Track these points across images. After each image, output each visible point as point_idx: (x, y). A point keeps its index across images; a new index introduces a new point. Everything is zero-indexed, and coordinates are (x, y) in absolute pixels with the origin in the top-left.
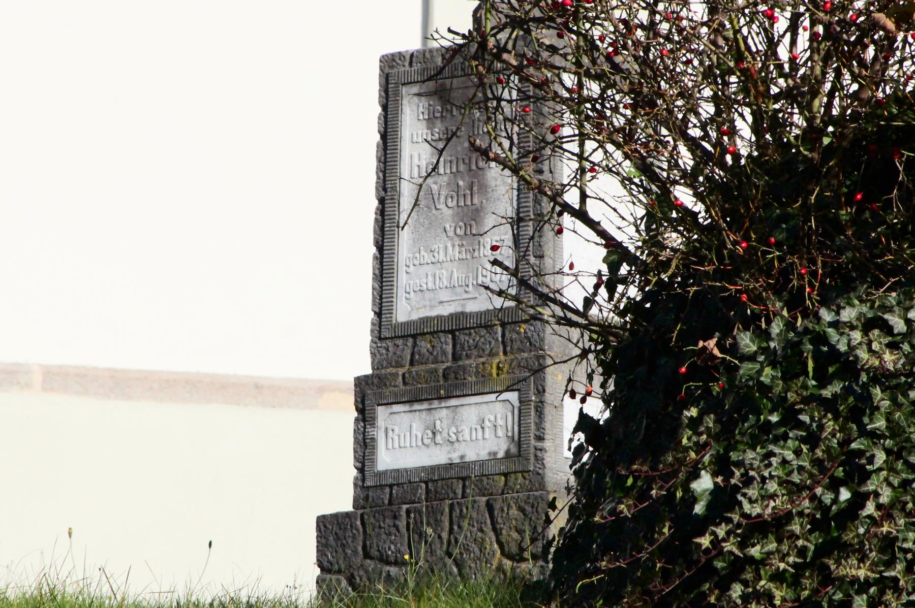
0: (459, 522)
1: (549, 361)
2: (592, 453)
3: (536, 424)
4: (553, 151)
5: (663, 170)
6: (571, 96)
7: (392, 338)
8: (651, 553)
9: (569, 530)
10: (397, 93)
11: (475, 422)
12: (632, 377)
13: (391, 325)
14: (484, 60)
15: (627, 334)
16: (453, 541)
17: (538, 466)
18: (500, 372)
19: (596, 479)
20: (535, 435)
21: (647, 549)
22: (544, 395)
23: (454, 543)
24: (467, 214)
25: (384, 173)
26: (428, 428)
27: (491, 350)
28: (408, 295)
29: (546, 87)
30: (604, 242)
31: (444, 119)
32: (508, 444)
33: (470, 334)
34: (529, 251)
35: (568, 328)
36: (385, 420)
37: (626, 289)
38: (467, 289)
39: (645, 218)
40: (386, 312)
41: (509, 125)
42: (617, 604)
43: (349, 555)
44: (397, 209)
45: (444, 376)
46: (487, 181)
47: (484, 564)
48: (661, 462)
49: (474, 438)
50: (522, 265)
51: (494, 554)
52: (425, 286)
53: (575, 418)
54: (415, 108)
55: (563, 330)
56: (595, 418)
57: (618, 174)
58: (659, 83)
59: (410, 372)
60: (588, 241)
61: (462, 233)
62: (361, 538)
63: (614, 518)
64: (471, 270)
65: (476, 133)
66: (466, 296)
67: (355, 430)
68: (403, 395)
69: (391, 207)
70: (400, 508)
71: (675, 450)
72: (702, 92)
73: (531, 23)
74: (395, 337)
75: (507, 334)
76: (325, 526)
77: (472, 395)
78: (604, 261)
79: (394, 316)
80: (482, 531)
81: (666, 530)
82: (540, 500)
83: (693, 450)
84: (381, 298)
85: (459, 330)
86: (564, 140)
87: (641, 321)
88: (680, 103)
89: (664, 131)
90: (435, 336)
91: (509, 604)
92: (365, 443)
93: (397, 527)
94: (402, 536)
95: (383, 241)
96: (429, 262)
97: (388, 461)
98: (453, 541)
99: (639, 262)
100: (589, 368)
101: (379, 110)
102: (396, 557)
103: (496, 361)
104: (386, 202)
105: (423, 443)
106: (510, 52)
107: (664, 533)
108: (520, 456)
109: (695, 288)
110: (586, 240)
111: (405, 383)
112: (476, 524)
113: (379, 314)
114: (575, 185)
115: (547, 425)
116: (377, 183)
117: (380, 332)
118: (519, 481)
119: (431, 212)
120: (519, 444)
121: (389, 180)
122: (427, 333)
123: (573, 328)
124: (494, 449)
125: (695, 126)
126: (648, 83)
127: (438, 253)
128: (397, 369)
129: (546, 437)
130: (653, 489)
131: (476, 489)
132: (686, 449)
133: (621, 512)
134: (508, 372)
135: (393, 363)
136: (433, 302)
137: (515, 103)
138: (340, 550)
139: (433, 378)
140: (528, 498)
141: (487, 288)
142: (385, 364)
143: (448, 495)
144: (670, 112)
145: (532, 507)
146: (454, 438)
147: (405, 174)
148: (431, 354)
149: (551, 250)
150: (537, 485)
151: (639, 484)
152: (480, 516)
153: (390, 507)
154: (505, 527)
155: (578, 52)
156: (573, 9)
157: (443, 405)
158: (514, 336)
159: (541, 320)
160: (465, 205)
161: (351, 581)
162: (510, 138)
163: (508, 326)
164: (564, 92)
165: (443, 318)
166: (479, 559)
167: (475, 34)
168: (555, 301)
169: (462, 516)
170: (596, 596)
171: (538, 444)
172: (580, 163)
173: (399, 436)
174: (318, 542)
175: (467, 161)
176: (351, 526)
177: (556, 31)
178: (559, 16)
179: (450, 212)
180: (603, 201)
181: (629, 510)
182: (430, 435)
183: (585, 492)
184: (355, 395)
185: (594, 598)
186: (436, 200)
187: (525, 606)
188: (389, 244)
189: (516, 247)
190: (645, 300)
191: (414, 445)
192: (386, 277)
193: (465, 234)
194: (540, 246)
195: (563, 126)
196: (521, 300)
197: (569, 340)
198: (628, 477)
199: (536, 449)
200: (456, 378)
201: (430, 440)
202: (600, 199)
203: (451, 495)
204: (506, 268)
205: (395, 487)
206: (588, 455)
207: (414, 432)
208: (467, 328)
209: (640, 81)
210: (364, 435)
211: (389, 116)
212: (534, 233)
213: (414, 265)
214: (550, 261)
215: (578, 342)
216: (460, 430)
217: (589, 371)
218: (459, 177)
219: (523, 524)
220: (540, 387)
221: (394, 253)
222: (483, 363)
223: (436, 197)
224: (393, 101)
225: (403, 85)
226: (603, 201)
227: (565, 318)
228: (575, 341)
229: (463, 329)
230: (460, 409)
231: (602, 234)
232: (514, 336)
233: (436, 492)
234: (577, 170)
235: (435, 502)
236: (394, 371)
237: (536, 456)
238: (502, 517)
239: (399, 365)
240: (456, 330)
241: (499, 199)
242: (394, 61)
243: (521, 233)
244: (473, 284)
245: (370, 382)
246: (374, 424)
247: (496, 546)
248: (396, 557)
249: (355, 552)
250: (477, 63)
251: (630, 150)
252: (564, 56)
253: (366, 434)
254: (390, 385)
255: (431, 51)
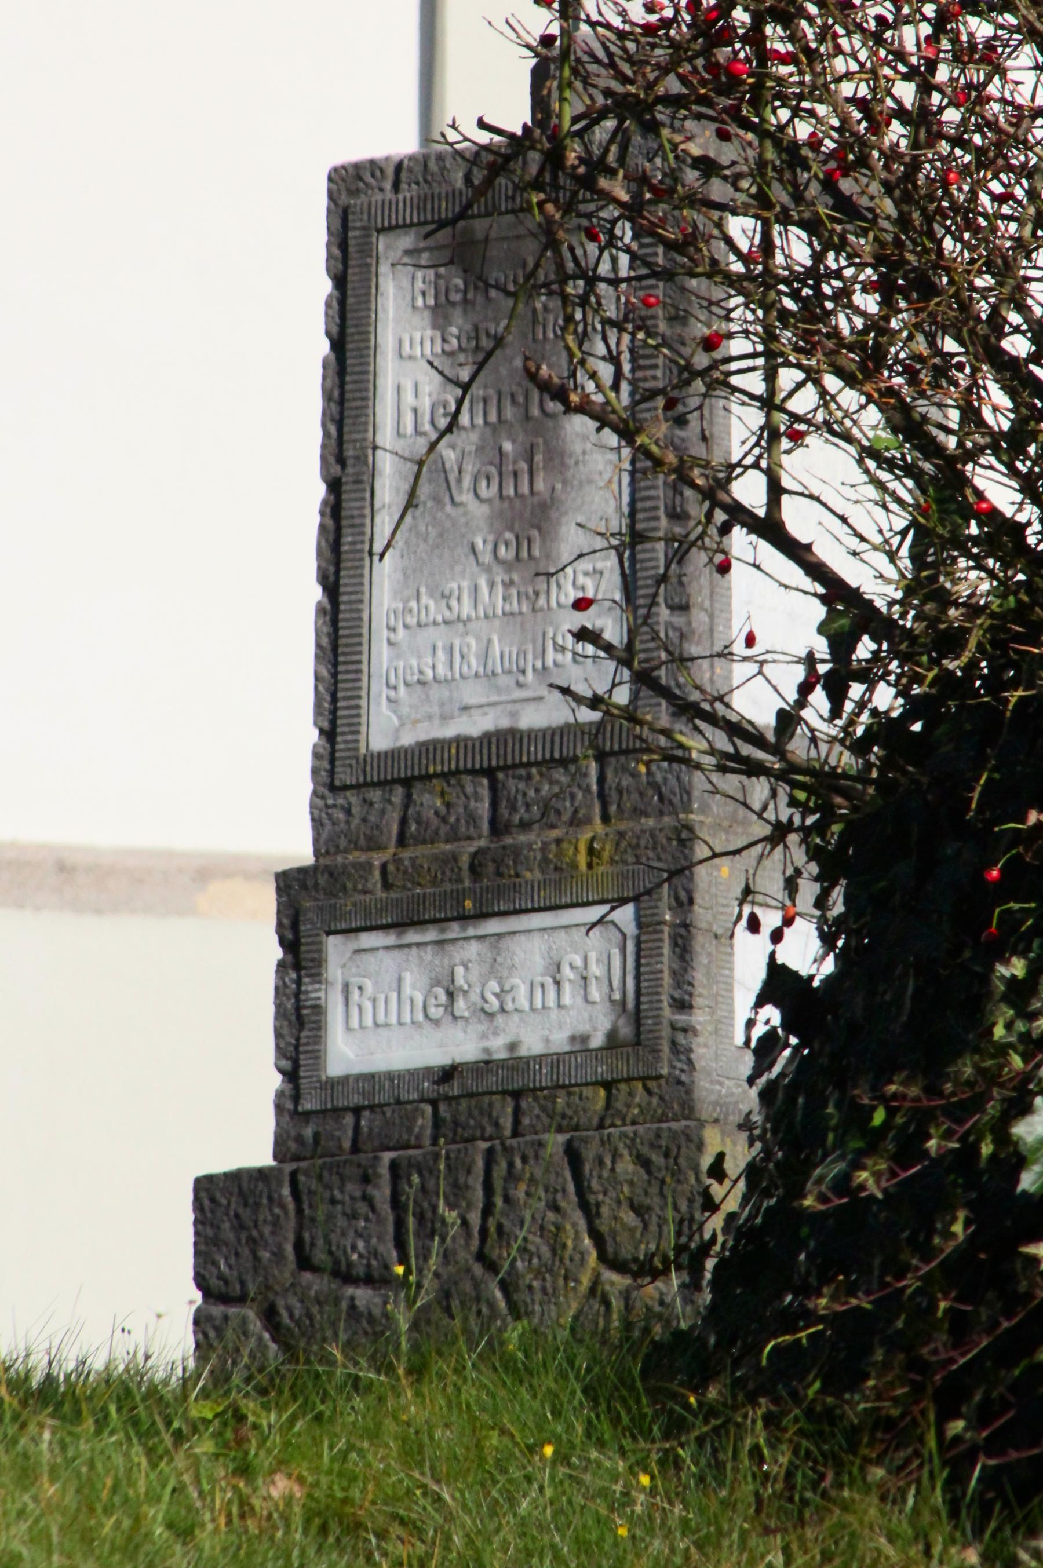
0: (505, 1189)
1: (701, 851)
2: (797, 1049)
3: (674, 973)
5: (949, 431)
7: (357, 787)
8: (927, 1279)
10: (367, 250)
12: (882, 884)
13: (357, 758)
15: (871, 790)
16: (492, 1229)
17: (679, 1065)
18: (595, 860)
20: (672, 997)
21: (917, 1269)
22: (690, 911)
23: (495, 1236)
26: (437, 983)
27: (576, 812)
28: (392, 693)
30: (821, 590)
31: (469, 307)
32: (613, 1017)
33: (529, 777)
35: (744, 778)
37: (871, 689)
39: (911, 533)
40: (346, 729)
41: (612, 335)
48: (947, 1078)
49: (538, 1003)
50: (642, 642)
53: (760, 974)
54: (406, 283)
55: (731, 782)
56: (804, 973)
57: (848, 438)
59: (397, 860)
60: (786, 587)
61: (511, 555)
62: (291, 1223)
63: (845, 1200)
64: (530, 636)
66: (519, 694)
67: (277, 988)
68: (382, 910)
70: (376, 1158)
71: (976, 1050)
72: (1034, 255)
74: (366, 785)
75: (610, 774)
76: (213, 1200)
77: (534, 910)
78: (822, 629)
79: (362, 737)
80: (556, 1208)
81: (958, 1228)
82: (683, 1141)
83: (1016, 1052)
84: (334, 699)
85: (505, 768)
86: (734, 366)
87: (901, 762)
88: (983, 281)
89: (950, 345)
90: (453, 781)
91: (617, 1389)
92: (299, 1017)
93: (367, 1198)
94: (380, 1221)
96: (439, 619)
97: (351, 1055)
98: (492, 1229)
99: (898, 632)
102: (369, 1265)
103: (585, 836)
105: (426, 1016)
107: (954, 1235)
108: (638, 1043)
109: (1020, 693)
110: (781, 584)
111: (387, 885)
113: (329, 734)
114: (756, 465)
115: (699, 976)
116: (324, 446)
117: (332, 773)
118: (637, 1100)
119: (442, 509)
122: (436, 775)
123: (754, 779)
124: (584, 1028)
125: (1017, 330)
126: (915, 243)
127: (459, 599)
129: (698, 1001)
130: (929, 1137)
132: (1002, 1050)
133: (862, 1187)
134: (612, 861)
137: (624, 286)
138: (246, 1252)
139: (448, 873)
140: (658, 1136)
141: (566, 691)
142: (343, 843)
143: (483, 1129)
144: (965, 307)
145: (667, 1155)
146: (494, 1003)
147: (386, 436)
148: (444, 820)
149: (706, 592)
150: (676, 1106)
151: (899, 1120)
152: (553, 1177)
153: (354, 1157)
154: (607, 1200)
155: (763, 175)
156: (751, 80)
157: (471, 932)
158: (626, 781)
161: (270, 1316)
162: (613, 359)
163: (613, 760)
165: (470, 744)
166: (550, 1271)
168: (712, 719)
169: (511, 1175)
170: (808, 1371)
171: (677, 1017)
173: (374, 1001)
174: (197, 1234)
176: (270, 1199)
177: (714, 126)
178: (720, 93)
179: (485, 509)
180: (817, 499)
182: (443, 998)
183: (781, 1135)
184: (279, 912)
186: (453, 483)
190: (908, 716)
194: (681, 583)
195: (730, 336)
197: (745, 804)
198: (874, 1108)
199: (674, 1027)
200: (499, 874)
201: (441, 1010)
202: (811, 497)
203: (489, 1130)
204: (608, 648)
205: (366, 1113)
206: (787, 1052)
207: (407, 990)
209: (897, 238)
212: (667, 567)
214: (703, 617)
215: (765, 808)
216: (507, 987)
217: (790, 872)
218: (503, 434)
219: (646, 1193)
220: (683, 895)
222: (558, 841)
224: (360, 266)
225: (379, 231)
226: (817, 499)
227: (736, 757)
228: (757, 806)
229: (514, 766)
230: (506, 943)
231: (817, 570)
232: (626, 781)
233: (456, 1123)
234: (762, 429)
236: (363, 857)
237: (674, 1043)
238: (600, 1177)
239: (374, 845)
240: (499, 768)
243: (639, 557)
245: (310, 883)
246: (319, 974)
247: (587, 1241)
249: (278, 1255)
250: (542, 196)
251: (879, 390)
252: (734, 181)
253: (302, 997)
254: (355, 889)
255: (440, 157)
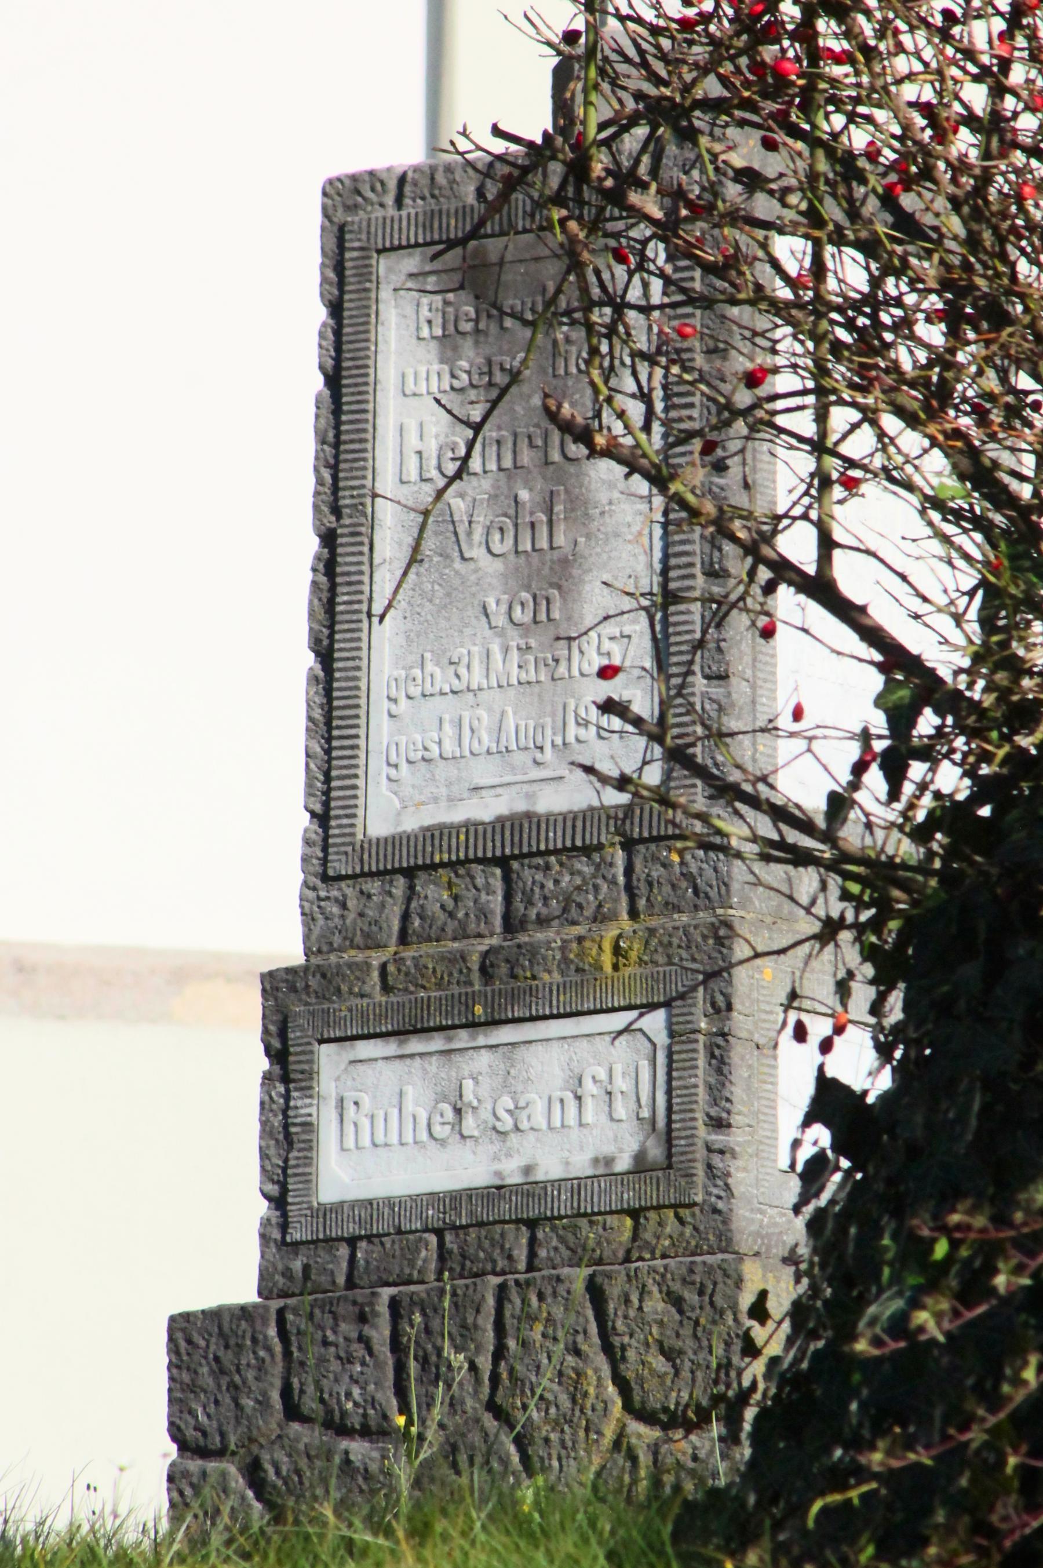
2: (848, 1173)
3: (710, 1087)
4: (752, 428)
5: (1022, 478)
6: (796, 294)
7: (354, 877)
9: (792, 1365)
10: (365, 274)
11: (559, 1082)
13: (353, 844)
14: (581, 203)
15: (933, 882)
16: (505, 1375)
17: (715, 1191)
19: (860, 1238)
20: (708, 1115)
24: (539, 570)
25: (335, 469)
26: (443, 1098)
28: (393, 772)
29: (733, 273)
30: (878, 657)
31: (482, 339)
33: (548, 867)
34: (693, 673)
35: (790, 868)
36: (338, 1079)
38: (539, 756)
40: (341, 812)
41: (643, 369)
42: (909, 1554)
43: (248, 1411)
44: (365, 559)
45: (483, 970)
46: (589, 490)
47: (582, 1434)
48: (1017, 1205)
51: (605, 1409)
52: (435, 749)
53: (809, 1089)
55: (776, 873)
56: (857, 1087)
57: (909, 486)
58: (1013, 265)
59: (398, 960)
60: (839, 653)
62: (278, 1369)
64: (549, 709)
65: (561, 372)
66: (536, 773)
67: (262, 1103)
68: (379, 1018)
69: (353, 554)
73: (697, 113)
74: (363, 875)
76: (189, 1341)
77: (552, 1017)
79: (359, 822)
80: (577, 1352)
84: (328, 778)
85: (522, 856)
86: (780, 404)
87: (968, 851)
92: (288, 1135)
93: (364, 1341)
94: (379, 1365)
95: (331, 636)
96: (447, 689)
98: (505, 1375)
100: (840, 965)
101: (321, 313)
102: (365, 1415)
103: (610, 933)
104: (340, 540)
106: (644, 186)
107: (1025, 1383)
108: (670, 1166)
110: (833, 651)
111: (386, 988)
112: (560, 1334)
113: (322, 818)
114: (805, 517)
115: (737, 1092)
116: (317, 494)
117: (325, 861)
118: (668, 1230)
120: (669, 1139)
121: (345, 489)
122: (442, 865)
123: (801, 869)
126: (986, 266)
128: (368, 953)
129: (736, 1119)
131: (562, 1248)
133: (921, 1329)
134: (641, 962)
135: (359, 939)
136: (455, 789)
137: (656, 314)
138: (226, 1400)
140: (691, 1271)
141: (589, 770)
142: (337, 940)
143: (494, 1262)
145: (701, 1293)
146: (508, 1123)
147: (386, 482)
148: (451, 915)
149: (748, 659)
151: (964, 1253)
154: (633, 1342)
155: (814, 189)
157: (481, 1041)
158: (657, 872)
159: (725, 849)
160: (534, 550)
162: (644, 396)
163: (641, 848)
164: (779, 283)
165: (480, 828)
167: (559, 140)
168: (754, 802)
171: (713, 1137)
172: (819, 460)
174: (172, 1379)
175: (539, 442)
176: (254, 1340)
177: (760, 133)
178: (765, 96)
179: (498, 565)
181: (939, 1324)
182: (450, 1115)
183: (830, 1270)
184: (264, 1017)
185: (853, 1541)
187: (681, 1557)
188: (348, 635)
189: (660, 668)
190: (976, 799)
191: (410, 1140)
192: (339, 727)
193: (535, 622)
194: (719, 649)
195: (776, 370)
196: (673, 799)
197: (791, 898)
198: (934, 1241)
200: (514, 976)
201: (448, 1127)
202: (868, 552)
203: (501, 1264)
204: (637, 722)
205: (363, 1244)
206: (837, 1177)
207: (409, 1107)
208: (540, 853)
210: (286, 1116)
211: (346, 330)
212: (704, 632)
213: (409, 697)
215: (813, 902)
216: (522, 1104)
219: (678, 1335)
220: (720, 1000)
221: (358, 668)
222: (580, 939)
223: (461, 530)
225: (379, 252)
227: (781, 845)
228: (805, 900)
229: (531, 855)
230: (522, 1052)
232: (657, 872)
234: (812, 475)
235: (462, 1282)
236: (360, 957)
237: (709, 1166)
238: (626, 1317)
240: (514, 857)
241: (617, 535)
242: (359, 193)
244: (553, 745)
245: (300, 985)
246: (311, 1088)
247: (611, 1389)
248: (365, 1415)
249: (264, 1403)
250: (564, 212)
254: (351, 992)
